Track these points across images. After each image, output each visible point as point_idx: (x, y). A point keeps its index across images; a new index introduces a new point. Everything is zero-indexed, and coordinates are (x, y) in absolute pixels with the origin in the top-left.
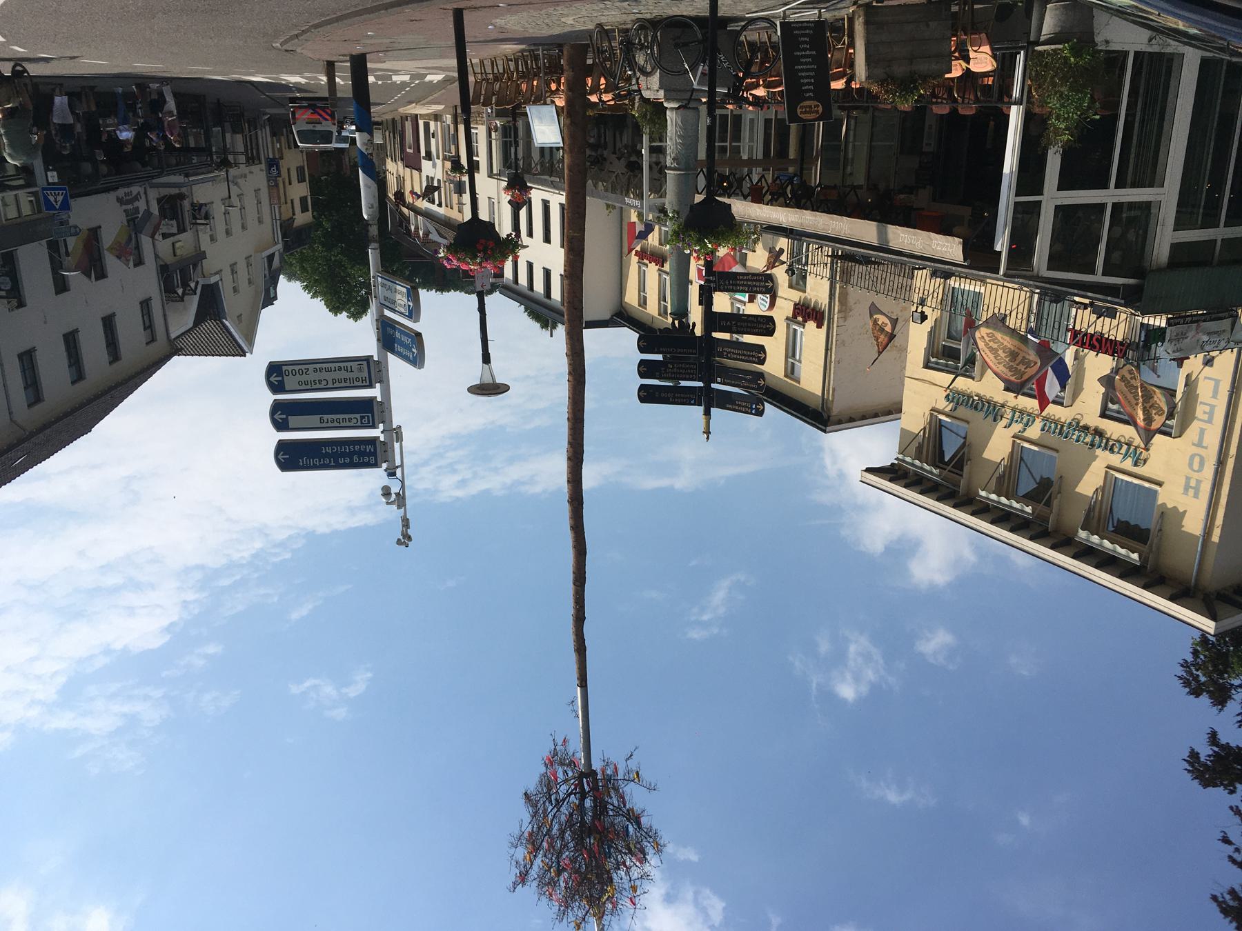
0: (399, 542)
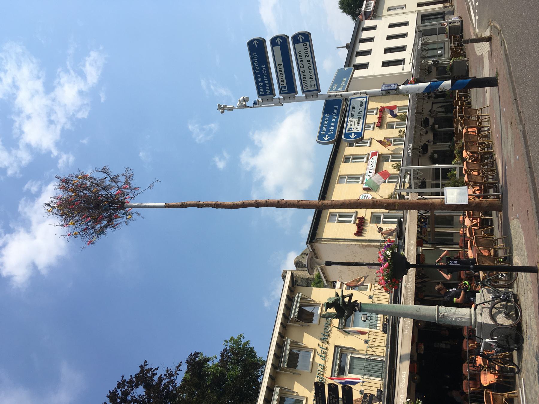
0: (219, 106)
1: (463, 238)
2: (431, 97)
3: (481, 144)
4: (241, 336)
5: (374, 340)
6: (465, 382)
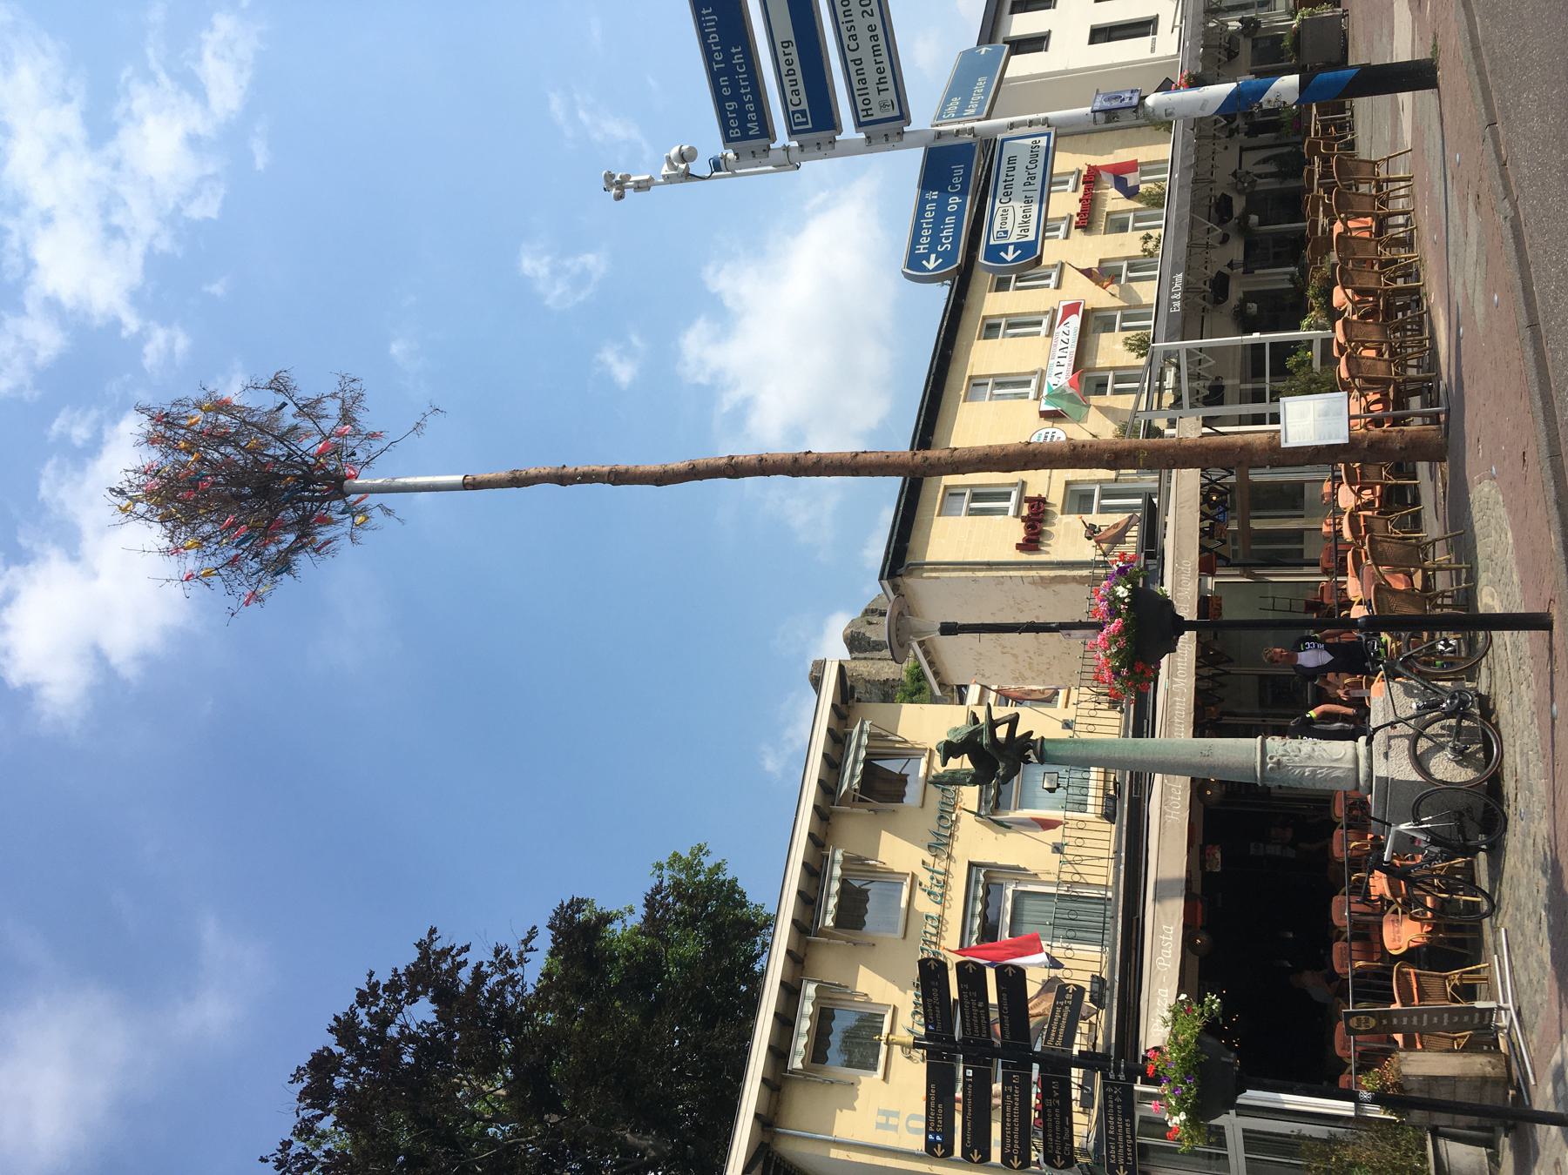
1: (1332, 544)
2: (1237, 130)
3: (1384, 264)
4: (701, 850)
5: (1079, 842)
6: (1337, 947)
